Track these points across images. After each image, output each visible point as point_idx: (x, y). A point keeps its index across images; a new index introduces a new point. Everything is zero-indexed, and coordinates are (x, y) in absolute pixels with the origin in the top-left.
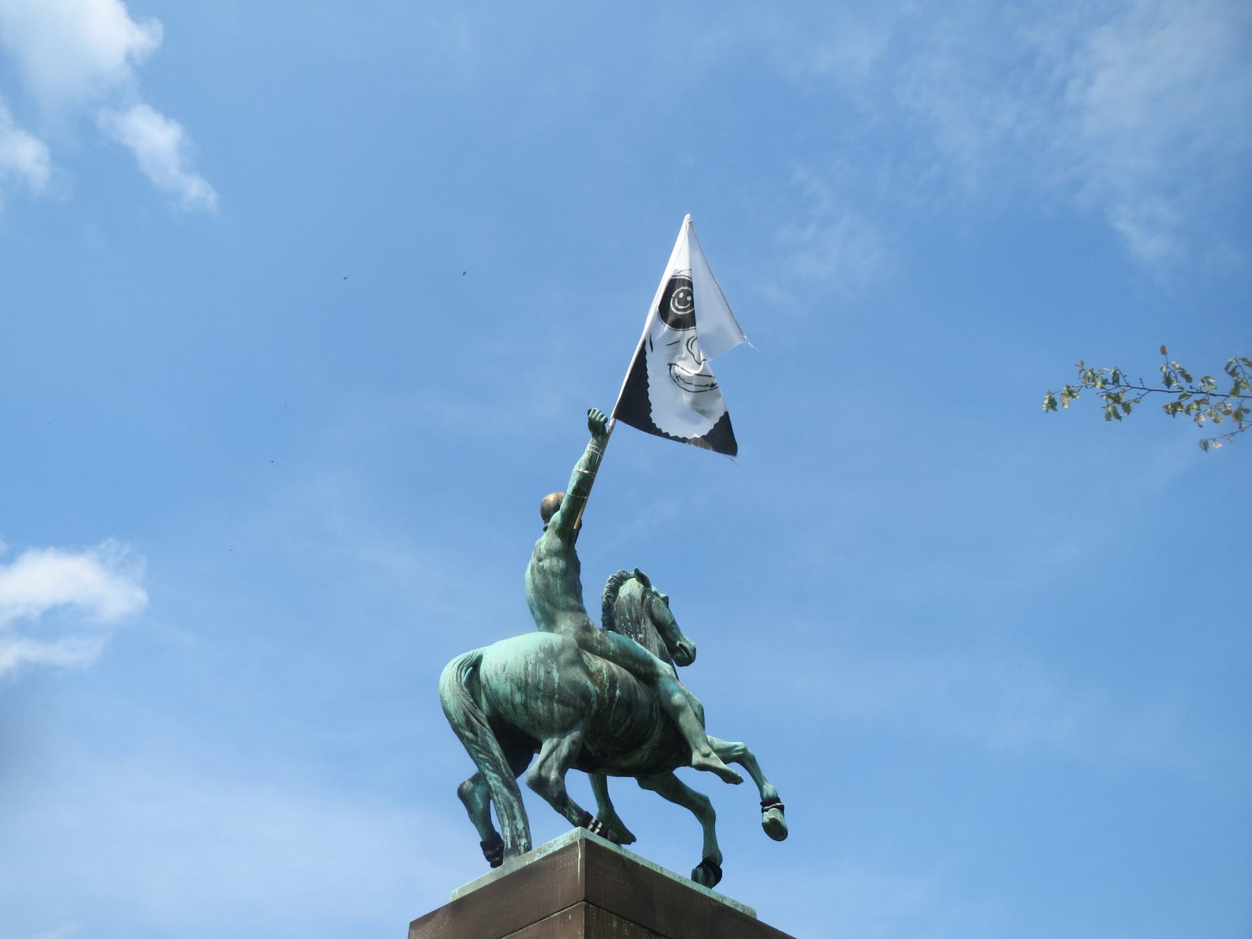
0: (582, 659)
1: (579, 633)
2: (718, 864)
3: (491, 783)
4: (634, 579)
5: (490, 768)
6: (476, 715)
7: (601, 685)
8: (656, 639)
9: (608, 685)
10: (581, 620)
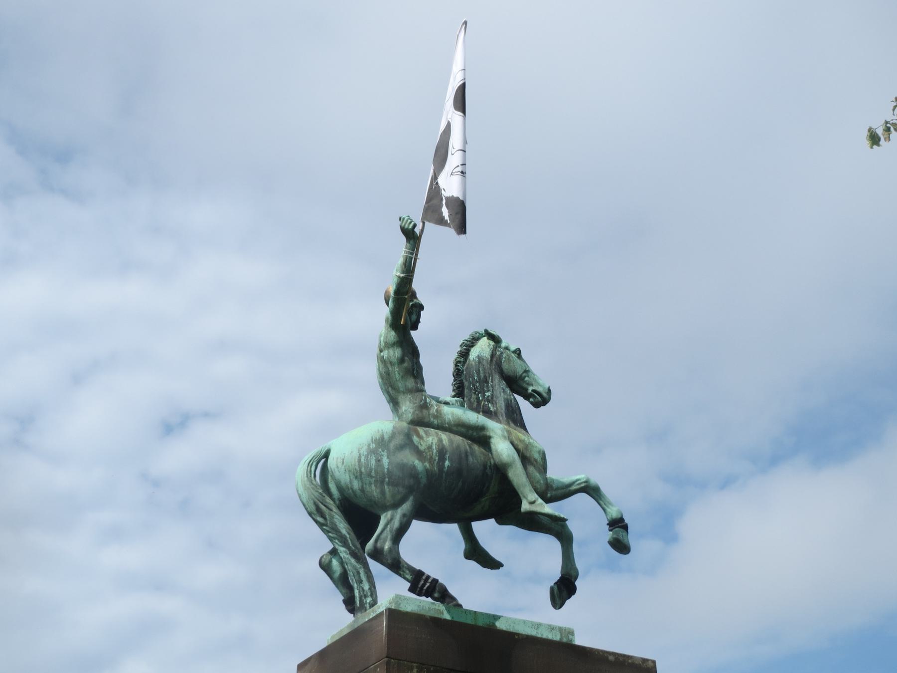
0: (412, 441)
1: (417, 412)
2: (573, 580)
3: (342, 555)
4: (486, 337)
5: (339, 543)
6: (324, 503)
7: (431, 460)
8: (502, 394)
9: (437, 458)
10: (418, 400)
